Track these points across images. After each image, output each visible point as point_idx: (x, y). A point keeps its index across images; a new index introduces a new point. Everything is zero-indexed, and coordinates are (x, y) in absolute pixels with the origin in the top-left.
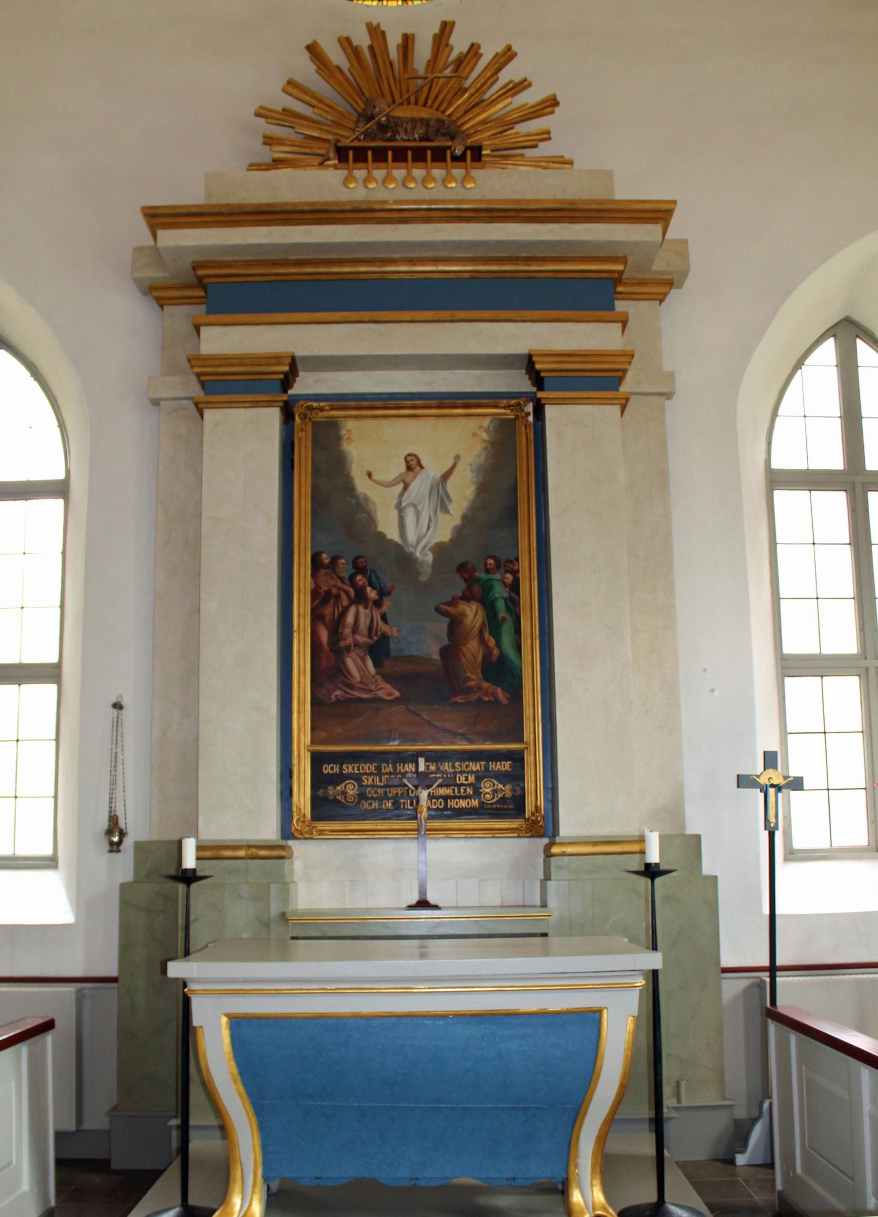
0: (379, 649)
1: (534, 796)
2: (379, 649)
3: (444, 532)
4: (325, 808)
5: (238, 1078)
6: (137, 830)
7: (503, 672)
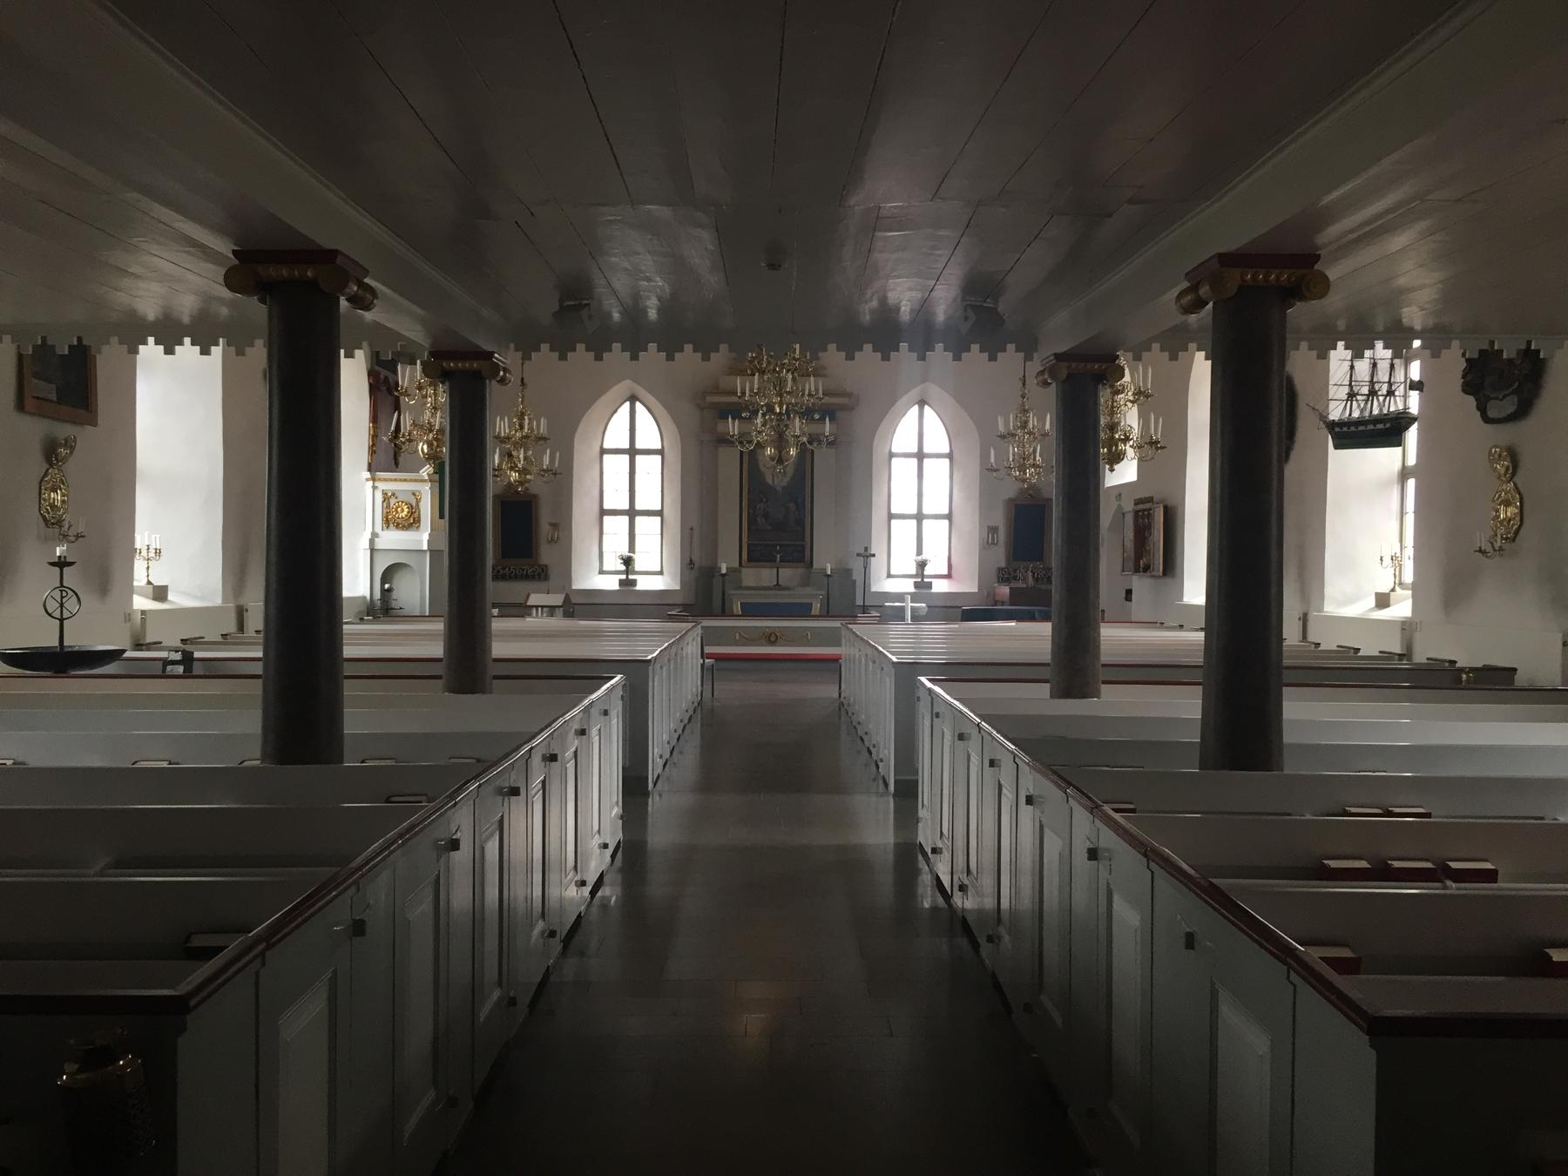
0: (766, 516)
1: (807, 558)
2: (766, 516)
3: (785, 481)
4: (750, 560)
5: (544, 528)
6: (695, 559)
7: (801, 523)
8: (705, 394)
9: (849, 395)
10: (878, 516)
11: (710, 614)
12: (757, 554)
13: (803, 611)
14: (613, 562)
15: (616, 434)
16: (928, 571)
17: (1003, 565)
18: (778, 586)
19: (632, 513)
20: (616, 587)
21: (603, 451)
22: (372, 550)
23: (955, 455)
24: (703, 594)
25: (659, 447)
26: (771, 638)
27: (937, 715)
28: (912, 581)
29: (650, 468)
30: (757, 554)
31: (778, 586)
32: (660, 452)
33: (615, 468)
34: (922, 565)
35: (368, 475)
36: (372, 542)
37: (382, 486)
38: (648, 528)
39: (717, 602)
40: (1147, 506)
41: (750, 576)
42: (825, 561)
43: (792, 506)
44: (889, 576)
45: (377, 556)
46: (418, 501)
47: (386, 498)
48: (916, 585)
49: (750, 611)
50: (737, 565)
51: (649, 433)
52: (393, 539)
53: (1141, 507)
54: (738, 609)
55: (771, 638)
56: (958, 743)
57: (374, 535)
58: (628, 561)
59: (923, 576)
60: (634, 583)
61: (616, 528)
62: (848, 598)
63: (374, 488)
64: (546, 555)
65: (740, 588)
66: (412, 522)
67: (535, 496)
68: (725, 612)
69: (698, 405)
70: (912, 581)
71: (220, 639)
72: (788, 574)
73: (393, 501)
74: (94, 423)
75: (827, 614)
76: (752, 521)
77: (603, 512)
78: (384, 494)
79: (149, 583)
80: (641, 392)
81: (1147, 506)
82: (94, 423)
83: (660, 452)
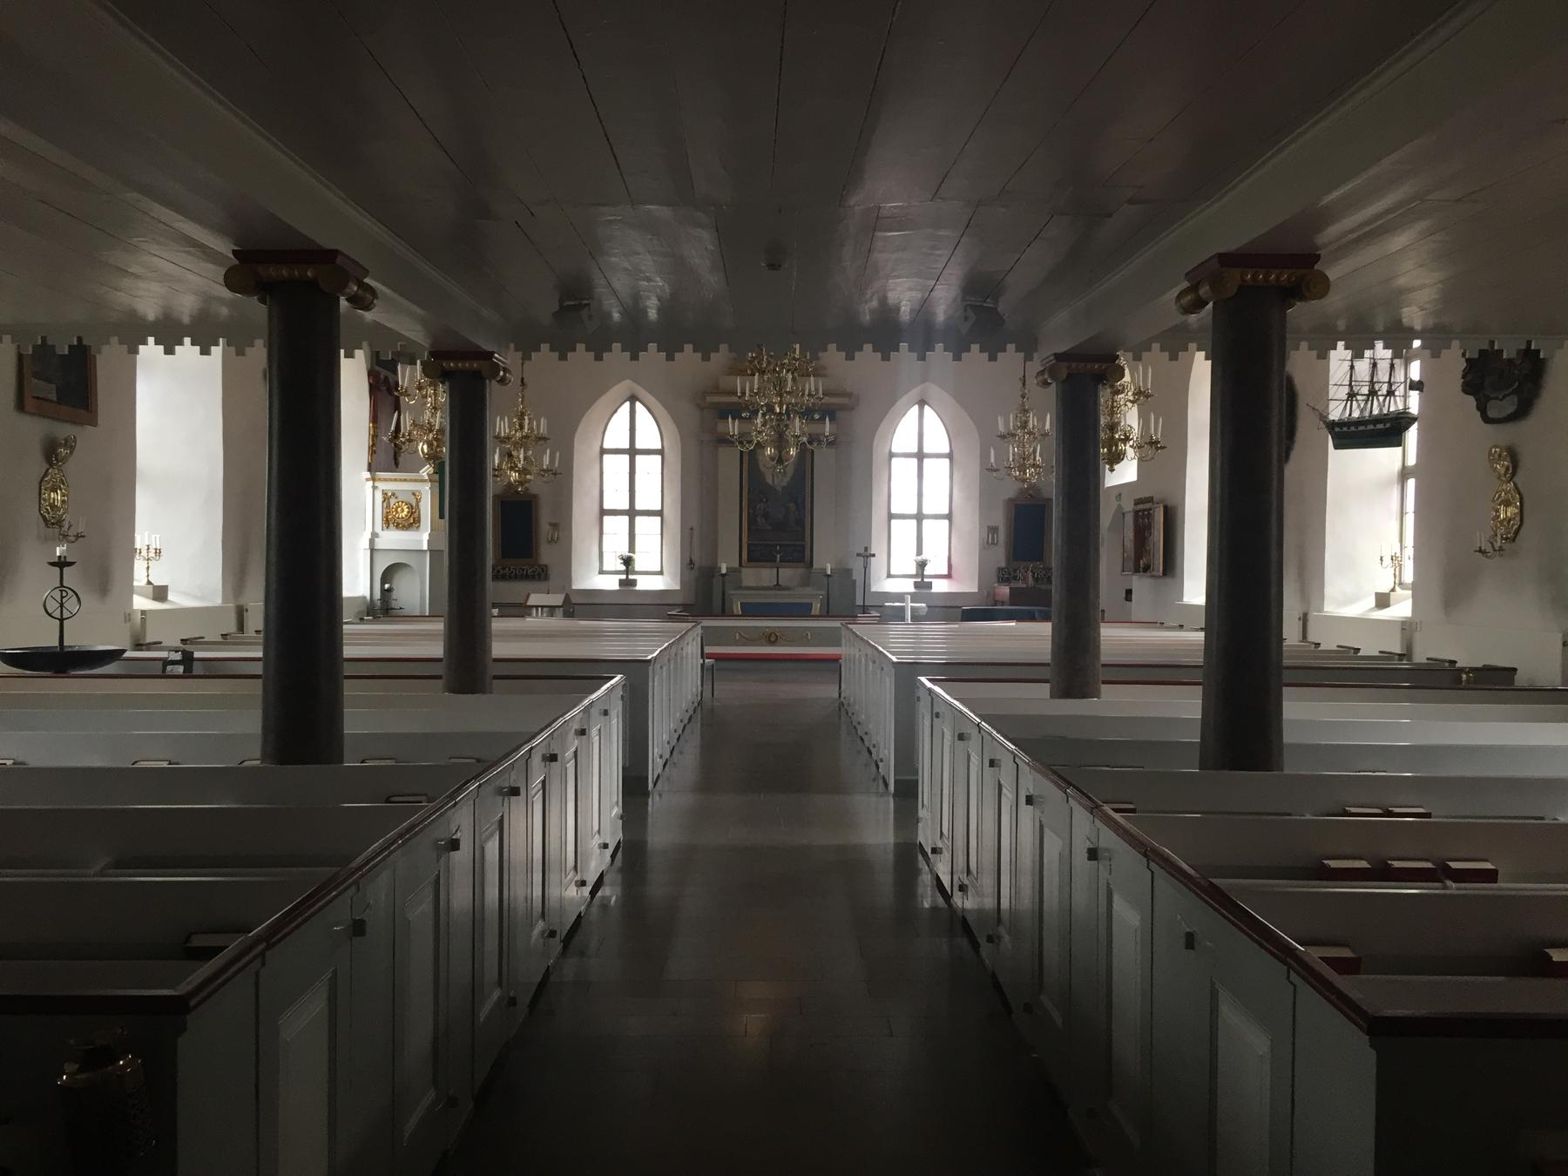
0: (766, 516)
1: (807, 558)
2: (766, 516)
3: (785, 481)
4: (750, 560)
5: (544, 528)
6: (695, 559)
7: (801, 523)
8: (705, 394)
9: (849, 395)
10: (878, 516)
11: (710, 614)
12: (757, 554)
13: (803, 611)
14: (613, 562)
15: (616, 434)
16: (928, 571)
17: (1003, 565)
18: (778, 586)
19: (632, 513)
20: (616, 587)
21: (603, 451)
22: (372, 550)
23: (955, 455)
24: (703, 594)
25: (659, 447)
26: (771, 638)
27: (937, 715)
28: (912, 581)
29: (650, 468)
30: (757, 554)
31: (778, 586)
32: (660, 452)
33: (615, 468)
34: (922, 565)
35: (368, 475)
36: (372, 542)
37: (382, 486)
38: (648, 528)
39: (717, 602)
40: (1147, 506)
41: (750, 576)
42: (825, 561)
43: (792, 506)
44: (889, 576)
45: (377, 556)
46: (418, 501)
47: (386, 498)
48: (916, 585)
49: (750, 611)
50: (737, 565)
51: (649, 433)
52: (393, 539)
53: (1141, 507)
54: (738, 609)
55: (771, 638)
56: (958, 743)
57: (374, 535)
58: (628, 561)
59: (923, 576)
60: (634, 583)
61: (616, 528)
62: (848, 598)
63: (374, 488)
64: (546, 555)
65: (740, 588)
66: (412, 522)
67: (535, 496)
68: (725, 612)
69: (698, 405)
70: (912, 581)
71: (220, 639)
72: (788, 574)
73: (393, 501)
74: (94, 423)
75: (827, 614)
76: (752, 521)
77: (603, 512)
78: (384, 494)
79: (149, 583)
80: (641, 392)
81: (1147, 506)
82: (94, 423)
83: (660, 452)
